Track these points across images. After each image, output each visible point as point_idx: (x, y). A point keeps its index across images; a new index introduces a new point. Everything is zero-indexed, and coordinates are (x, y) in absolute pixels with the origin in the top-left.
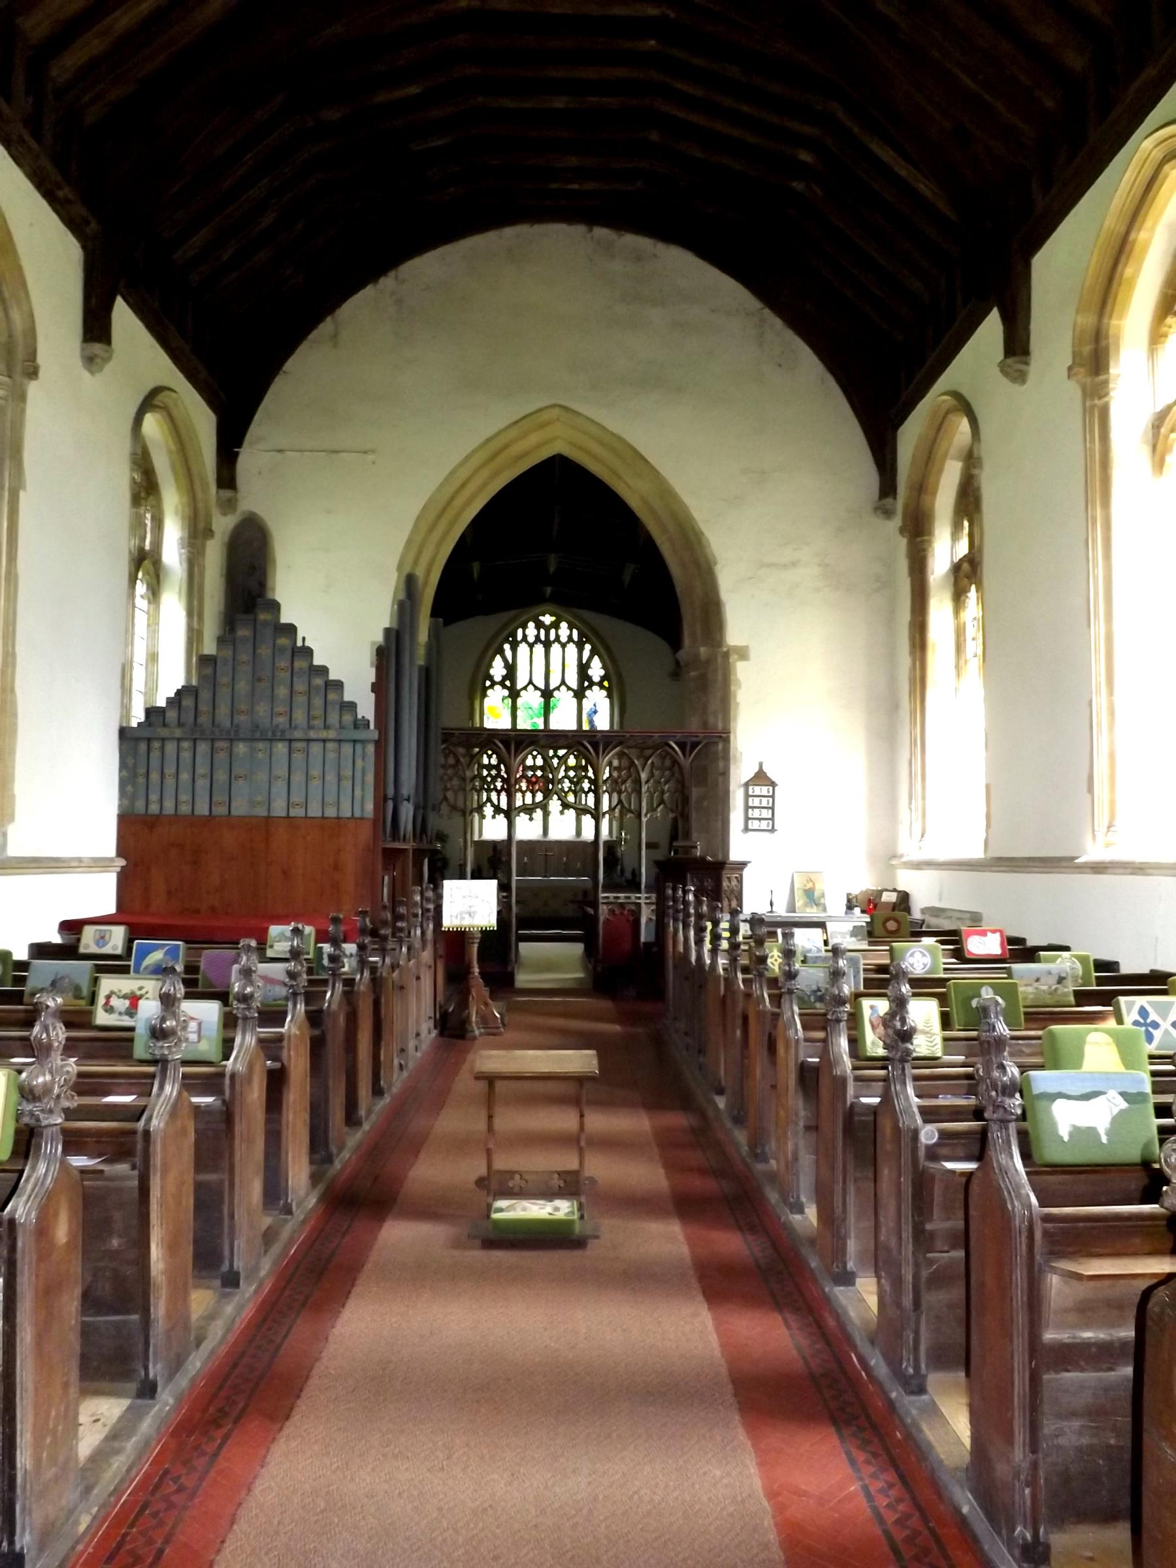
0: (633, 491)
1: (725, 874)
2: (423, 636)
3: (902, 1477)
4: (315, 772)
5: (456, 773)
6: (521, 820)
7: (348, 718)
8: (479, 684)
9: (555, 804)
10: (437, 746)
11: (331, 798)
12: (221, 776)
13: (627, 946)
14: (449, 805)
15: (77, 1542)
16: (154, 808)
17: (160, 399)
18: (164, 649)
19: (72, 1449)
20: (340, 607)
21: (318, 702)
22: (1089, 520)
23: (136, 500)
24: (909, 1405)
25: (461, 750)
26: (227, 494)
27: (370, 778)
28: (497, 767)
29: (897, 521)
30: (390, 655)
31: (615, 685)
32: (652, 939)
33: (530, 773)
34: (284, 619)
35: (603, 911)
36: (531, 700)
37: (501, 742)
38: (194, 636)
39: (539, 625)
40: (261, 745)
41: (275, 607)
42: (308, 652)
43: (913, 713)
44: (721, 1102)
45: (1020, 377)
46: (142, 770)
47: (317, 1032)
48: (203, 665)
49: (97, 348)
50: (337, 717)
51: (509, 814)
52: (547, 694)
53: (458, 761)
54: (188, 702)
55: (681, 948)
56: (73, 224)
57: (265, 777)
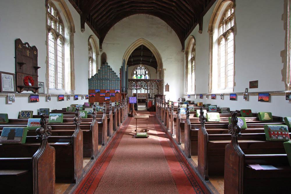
0: (152, 49)
1: (163, 96)
2: (126, 68)
3: (188, 169)
4: (113, 84)
6: (138, 90)
8: (133, 74)
9: (142, 88)
10: (128, 81)
11: (115, 87)
12: (101, 85)
13: (151, 105)
15: (83, 178)
16: (93, 89)
17: (92, 36)
18: (93, 69)
19: (82, 166)
20: (115, 64)
21: (113, 75)
22: (210, 51)
23: (89, 50)
24: (189, 159)
26: (101, 49)
28: (135, 84)
29: (184, 53)
30: (122, 70)
31: (149, 74)
32: (154, 104)
34: (108, 65)
35: (148, 101)
36: (139, 76)
38: (97, 67)
39: (140, 67)
40: (106, 81)
41: (107, 63)
42: (112, 69)
43: (186, 77)
44: (163, 123)
45: (201, 33)
47: (113, 115)
48: (98, 71)
49: (83, 29)
51: (137, 89)
52: (141, 75)
55: (158, 105)
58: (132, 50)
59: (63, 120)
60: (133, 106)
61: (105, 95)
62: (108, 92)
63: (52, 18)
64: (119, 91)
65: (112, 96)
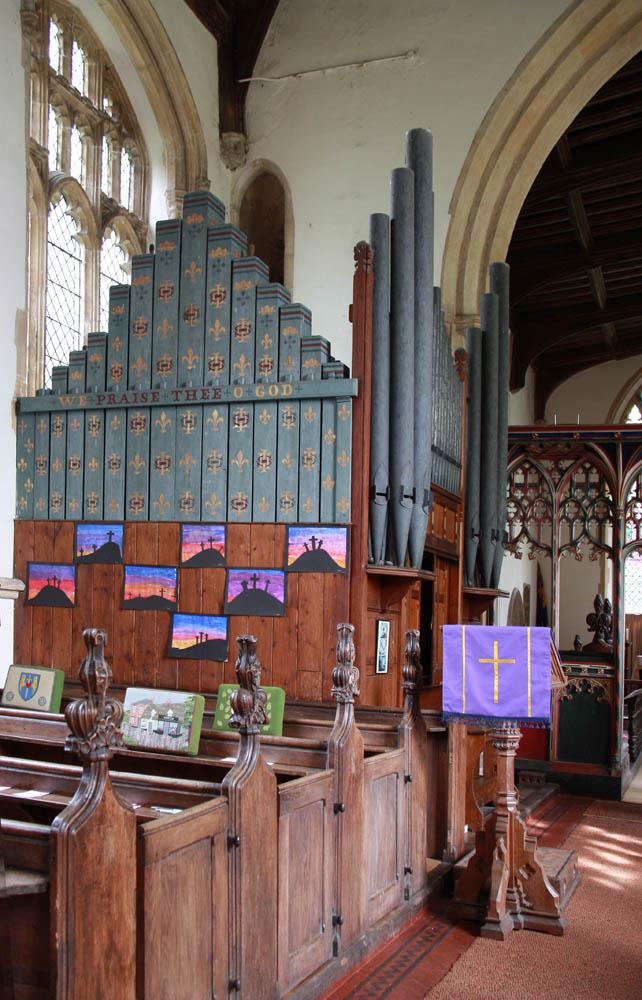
5: (540, 496)
7: (312, 364)
11: (287, 495)
12: (138, 463)
14: (529, 541)
16: (57, 511)
21: (268, 341)
25: (548, 464)
26: (235, 138)
27: (345, 460)
33: (519, 494)
37: (601, 446)
40: (189, 414)
46: (43, 458)
50: (295, 363)
53: (542, 479)
54: (96, 357)
56: (212, 27)
57: (196, 462)
58: (558, 100)
59: (204, 715)
60: (509, 763)
61: (169, 595)
62: (208, 558)
63: (72, 112)
64: (336, 545)
65: (255, 602)
